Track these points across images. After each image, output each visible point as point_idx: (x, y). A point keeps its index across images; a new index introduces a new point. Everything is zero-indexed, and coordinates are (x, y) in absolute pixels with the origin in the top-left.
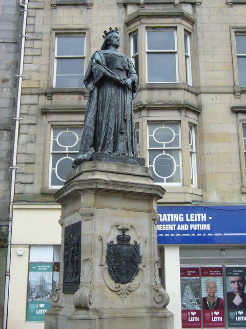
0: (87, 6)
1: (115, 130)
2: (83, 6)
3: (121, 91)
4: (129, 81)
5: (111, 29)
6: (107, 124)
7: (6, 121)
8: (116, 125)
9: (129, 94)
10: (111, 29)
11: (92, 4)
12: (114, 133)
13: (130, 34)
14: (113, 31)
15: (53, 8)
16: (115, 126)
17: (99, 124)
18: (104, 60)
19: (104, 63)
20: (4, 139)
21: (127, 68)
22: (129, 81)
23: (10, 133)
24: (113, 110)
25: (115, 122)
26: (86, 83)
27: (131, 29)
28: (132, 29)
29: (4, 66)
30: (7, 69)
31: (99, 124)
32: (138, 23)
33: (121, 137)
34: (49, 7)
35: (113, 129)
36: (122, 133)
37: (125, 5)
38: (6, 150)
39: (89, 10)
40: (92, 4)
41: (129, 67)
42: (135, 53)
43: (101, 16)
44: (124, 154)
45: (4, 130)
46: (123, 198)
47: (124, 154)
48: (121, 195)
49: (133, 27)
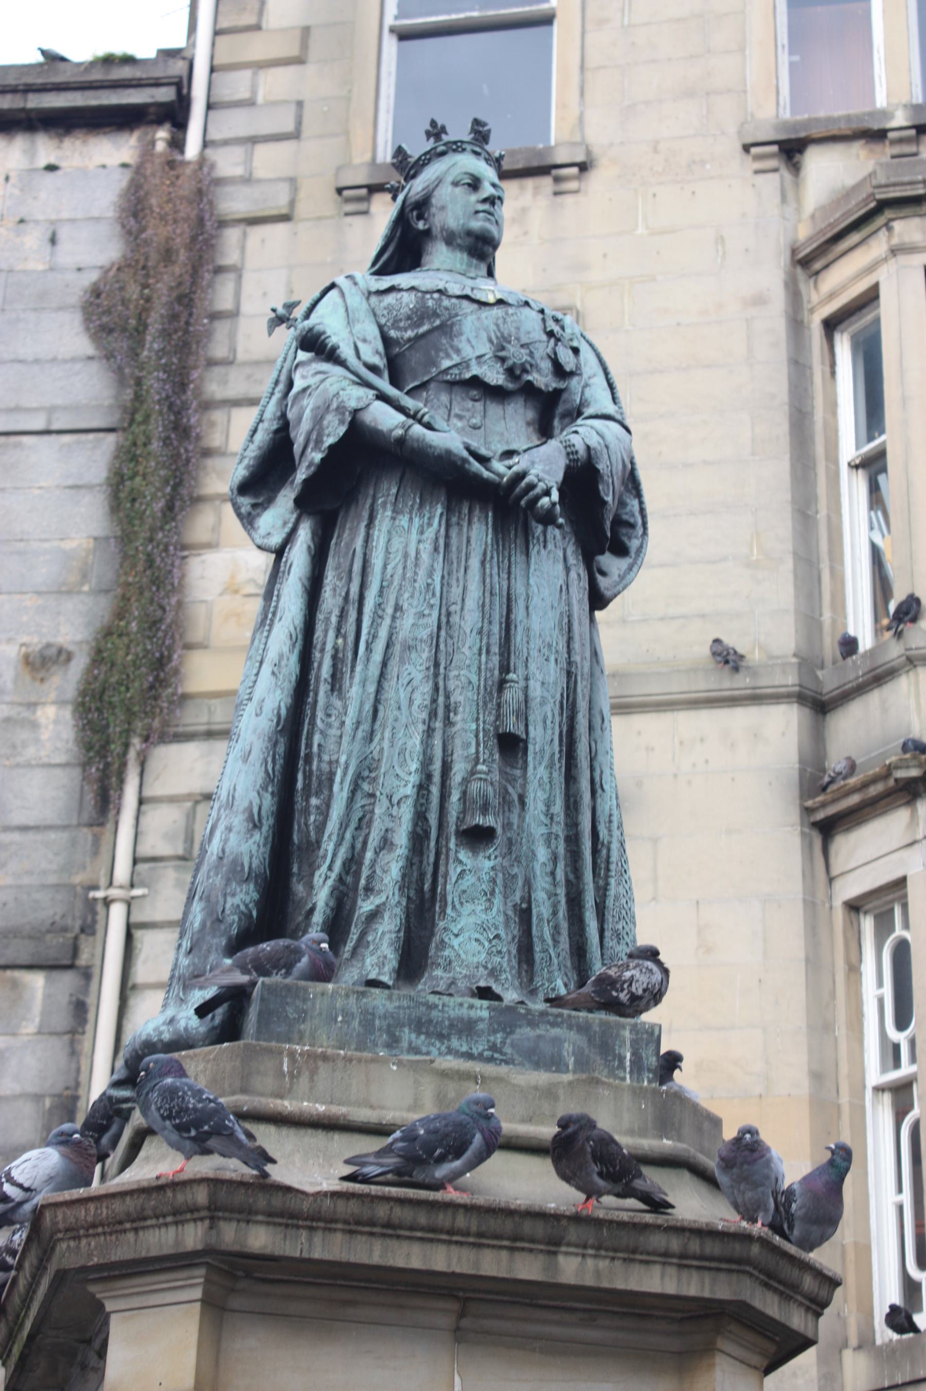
0: (557, 180)
1: (420, 817)
2: (530, 183)
3: (479, 533)
4: (544, 466)
5: (436, 131)
6: (366, 773)
7: (49, 908)
8: (433, 780)
9: (550, 569)
10: (436, 131)
11: (583, 167)
12: (418, 839)
13: (831, 325)
14: (457, 147)
15: (350, 207)
16: (423, 788)
17: (308, 776)
18: (372, 332)
19: (372, 352)
20: (30, 1027)
21: (543, 379)
22: (544, 466)
23: (67, 981)
24: (413, 671)
25: (426, 762)
26: (246, 502)
27: (832, 296)
28: (844, 287)
29: (44, 572)
30: (65, 591)
31: (308, 776)
32: (878, 246)
33: (469, 873)
34: (327, 202)
35: (406, 813)
36: (478, 837)
37: (791, 150)
38: (38, 1098)
39: (568, 200)
40: (583, 167)
41: (560, 371)
42: (870, 438)
43: (641, 230)
44: (485, 993)
45: (30, 967)
46: (459, 1335)
47: (485, 993)
48: (442, 1316)
49: (841, 280)
